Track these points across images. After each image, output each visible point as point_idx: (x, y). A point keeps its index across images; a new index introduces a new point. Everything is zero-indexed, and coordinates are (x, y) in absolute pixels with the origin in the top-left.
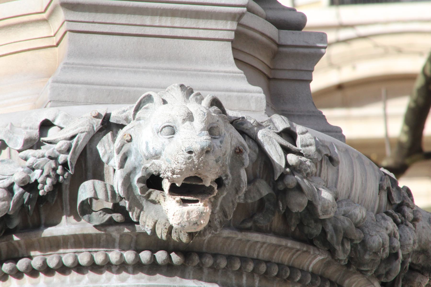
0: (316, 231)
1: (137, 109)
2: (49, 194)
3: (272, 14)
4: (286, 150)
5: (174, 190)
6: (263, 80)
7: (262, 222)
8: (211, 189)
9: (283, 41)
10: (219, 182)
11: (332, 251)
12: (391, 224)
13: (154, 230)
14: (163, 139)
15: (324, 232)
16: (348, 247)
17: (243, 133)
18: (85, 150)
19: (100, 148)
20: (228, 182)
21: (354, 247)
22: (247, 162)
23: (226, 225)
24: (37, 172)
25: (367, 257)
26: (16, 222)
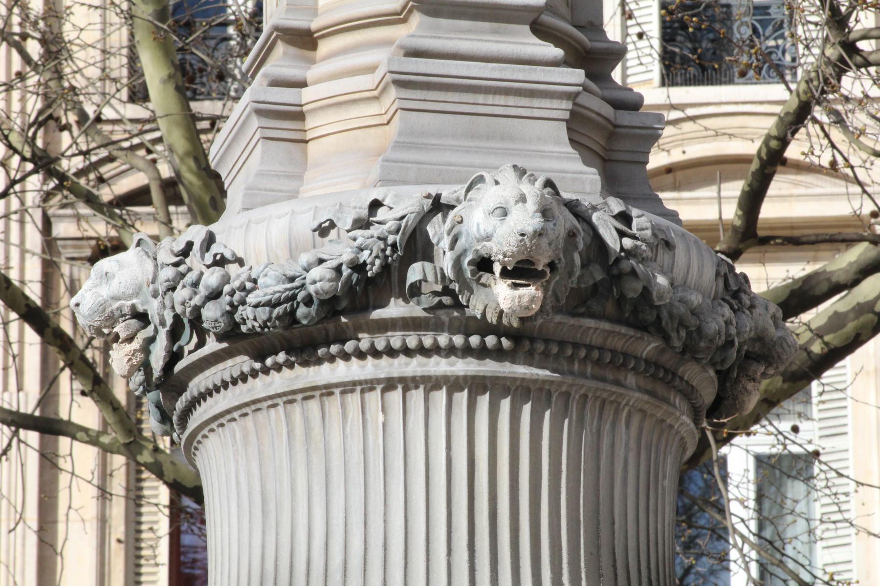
0: (651, 317)
1: (468, 190)
2: (378, 275)
3: (608, 93)
4: (622, 234)
6: (598, 161)
7: (595, 306)
8: (542, 274)
10: (552, 265)
11: (666, 338)
12: (727, 311)
13: (484, 314)
14: (495, 221)
15: (659, 319)
16: (683, 333)
19: (430, 230)
20: (561, 266)
21: (689, 334)
22: (581, 246)
24: (366, 253)
25: (702, 344)
26: (344, 304)
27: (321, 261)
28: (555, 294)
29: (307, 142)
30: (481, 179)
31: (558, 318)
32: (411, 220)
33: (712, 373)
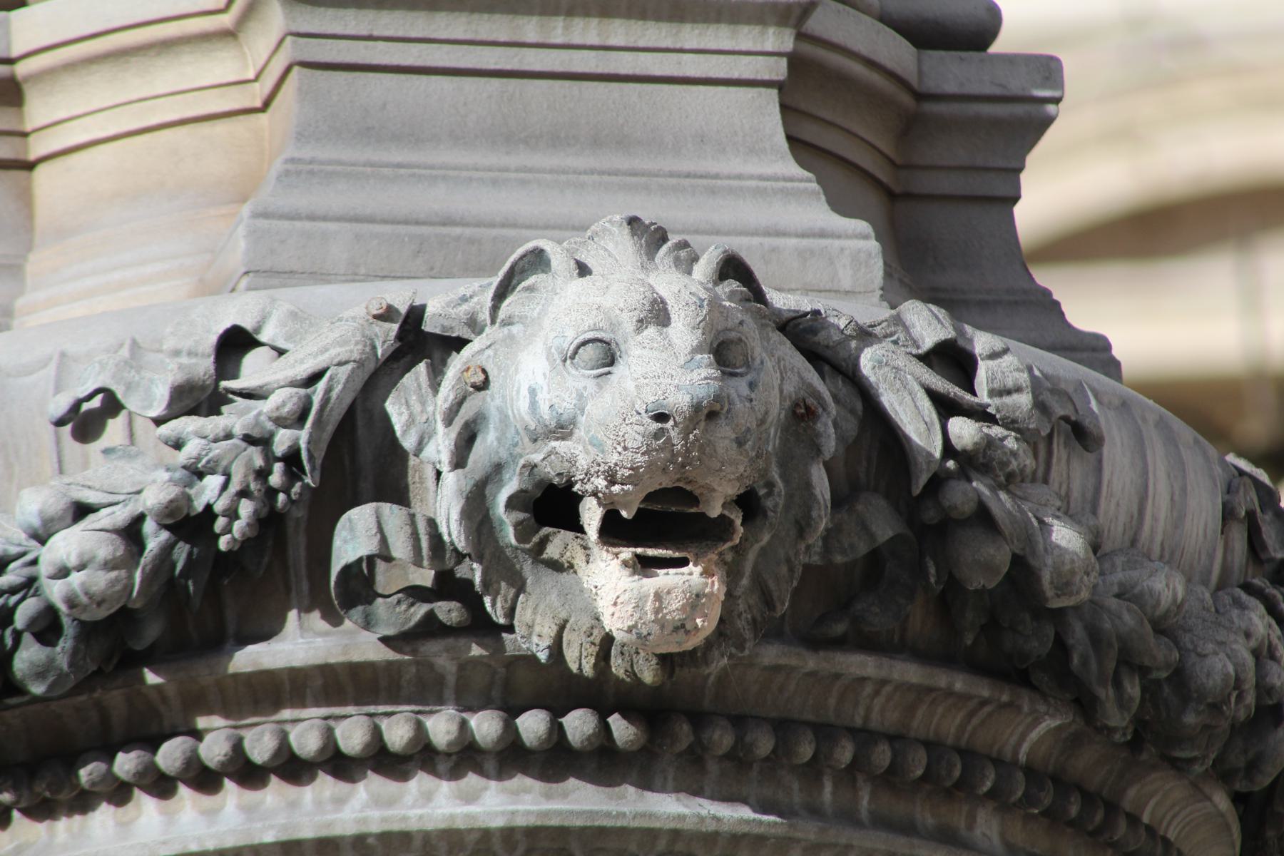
0: (1037, 644)
1: (501, 294)
2: (247, 545)
4: (946, 407)
5: (614, 530)
6: (873, 199)
7: (878, 618)
8: (721, 528)
9: (932, 84)
10: (748, 503)
11: (1085, 704)
13: (557, 648)
14: (580, 379)
15: (1061, 647)
16: (1133, 689)
17: (816, 357)
18: (351, 413)
19: (395, 410)
20: (775, 503)
21: (1151, 690)
22: (830, 445)
23: (770, 631)
24: (213, 483)
25: (1190, 719)
26: (152, 631)
27: (81, 511)
28: (759, 584)
29: (30, 166)
30: (537, 260)
31: (771, 654)
32: (339, 383)
33: (1222, 801)
